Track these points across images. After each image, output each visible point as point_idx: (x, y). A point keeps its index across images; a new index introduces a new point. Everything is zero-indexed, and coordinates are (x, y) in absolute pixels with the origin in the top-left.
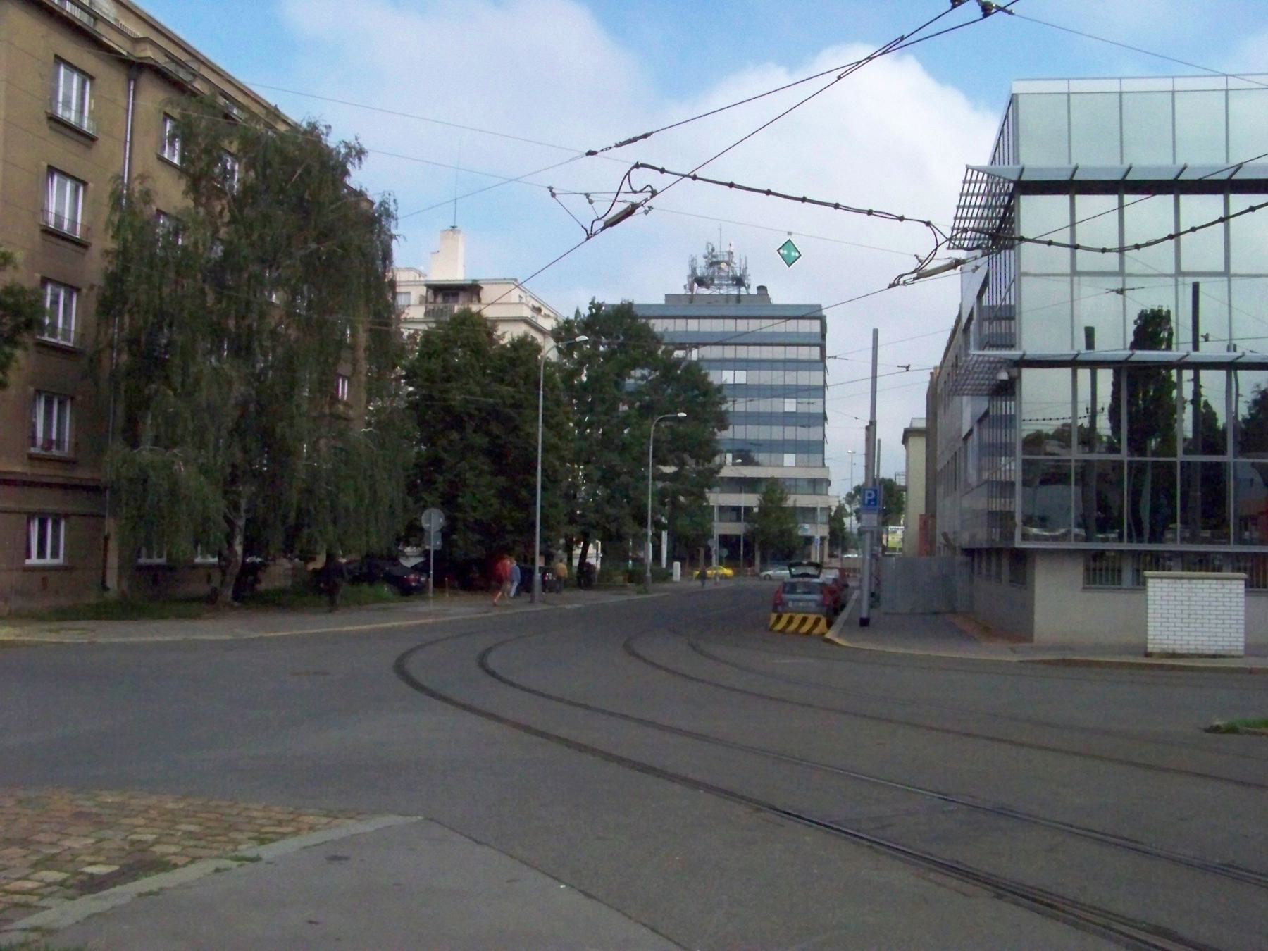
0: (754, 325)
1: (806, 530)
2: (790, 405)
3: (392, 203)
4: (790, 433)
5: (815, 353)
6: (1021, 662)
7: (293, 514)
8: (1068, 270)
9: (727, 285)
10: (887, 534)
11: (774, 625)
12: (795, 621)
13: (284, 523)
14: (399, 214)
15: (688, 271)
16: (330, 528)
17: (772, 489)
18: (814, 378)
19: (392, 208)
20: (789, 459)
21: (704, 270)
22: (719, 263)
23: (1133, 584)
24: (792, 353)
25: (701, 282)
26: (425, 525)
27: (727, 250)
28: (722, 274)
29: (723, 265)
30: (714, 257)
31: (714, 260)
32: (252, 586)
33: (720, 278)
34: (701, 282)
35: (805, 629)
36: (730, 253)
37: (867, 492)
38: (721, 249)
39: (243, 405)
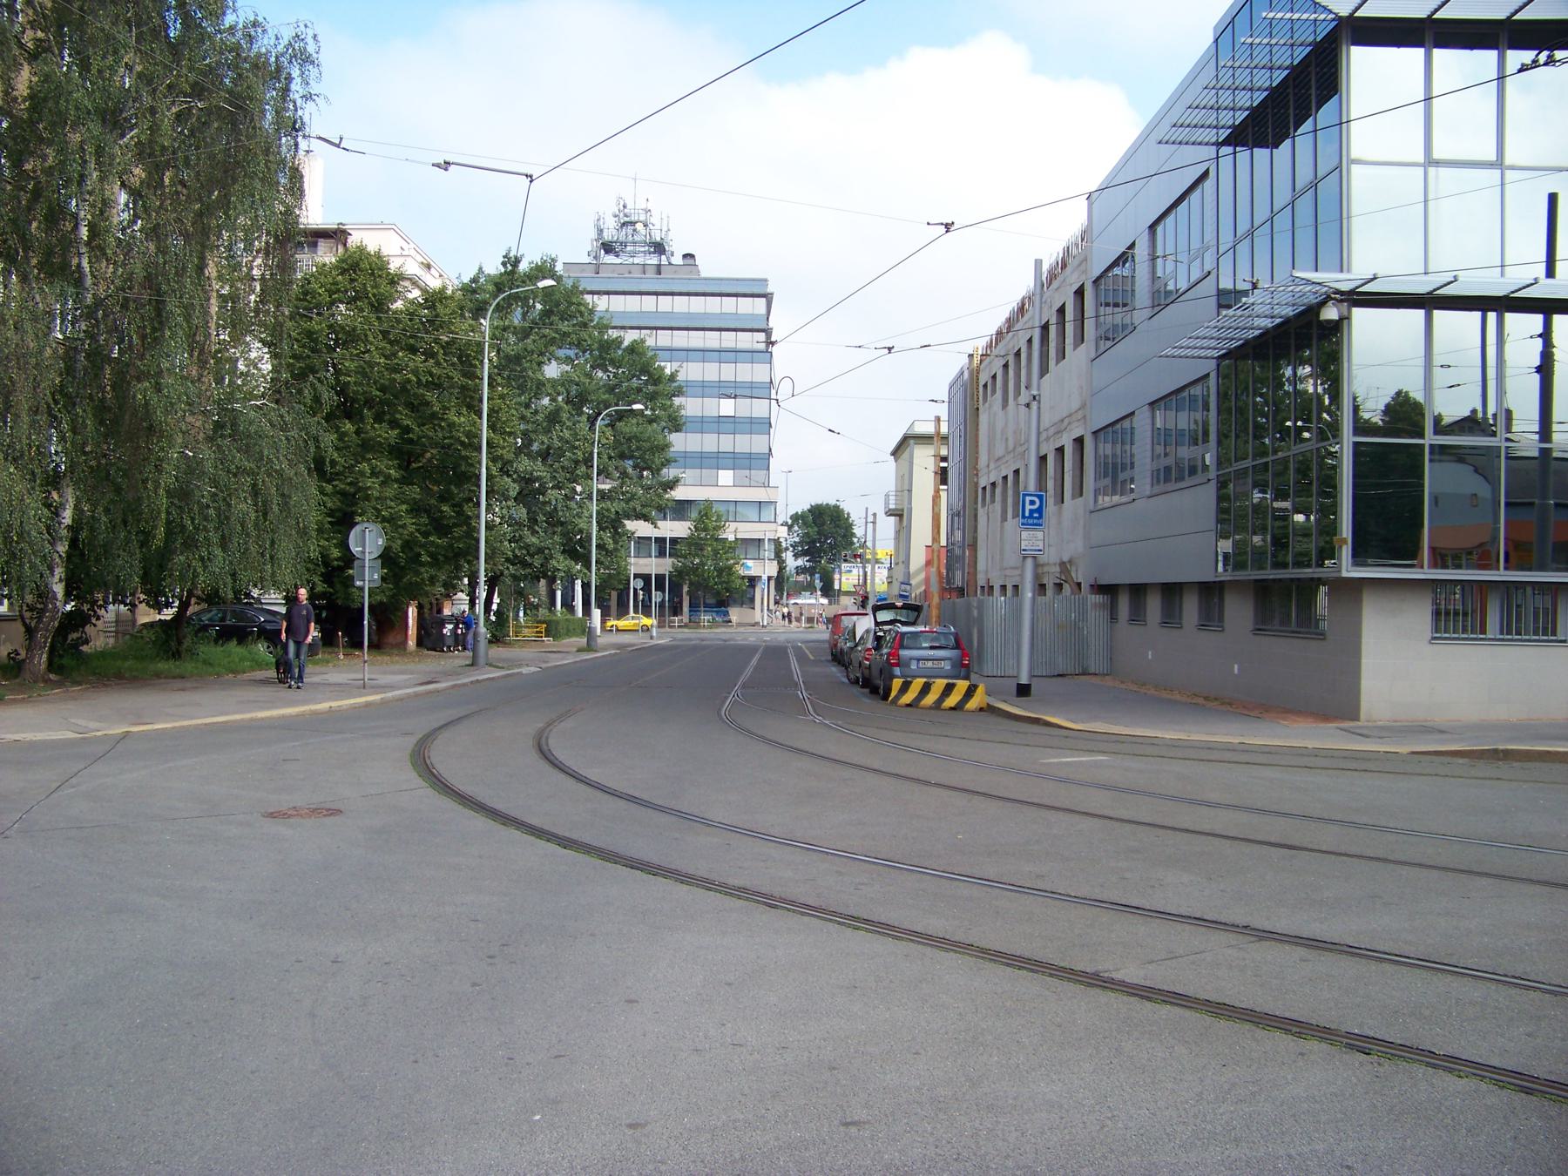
0: (681, 305)
1: (749, 568)
2: (727, 407)
3: (310, 40)
4: (726, 443)
5: (754, 341)
6: (1413, 753)
7: (160, 532)
8: (1421, 159)
9: (644, 252)
10: (840, 573)
11: (897, 697)
12: (934, 688)
13: (142, 545)
15: (593, 234)
16: (218, 551)
17: (706, 516)
18: (758, 373)
19: (311, 48)
20: (726, 477)
21: (615, 232)
22: (633, 223)
23: (1502, 633)
24: (729, 339)
25: (608, 248)
26: (356, 549)
27: (644, 206)
28: (637, 238)
29: (639, 226)
30: (626, 216)
31: (627, 219)
32: (76, 645)
33: (634, 243)
34: (608, 248)
35: (952, 701)
36: (647, 211)
37: (1028, 499)
38: (635, 209)
39: (70, 347)
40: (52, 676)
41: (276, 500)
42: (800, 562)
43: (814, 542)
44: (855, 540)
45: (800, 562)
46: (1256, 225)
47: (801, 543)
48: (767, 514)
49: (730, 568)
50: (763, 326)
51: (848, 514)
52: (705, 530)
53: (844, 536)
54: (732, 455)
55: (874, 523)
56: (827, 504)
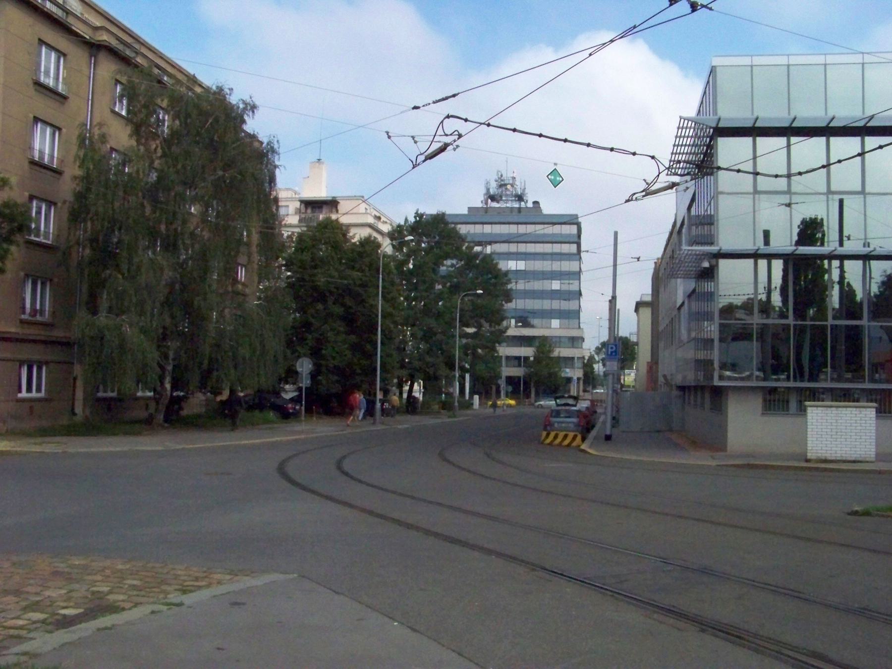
0: (530, 229)
1: (567, 373)
2: (556, 285)
3: (275, 143)
4: (556, 305)
5: (573, 248)
6: (718, 465)
7: (206, 362)
8: (751, 190)
9: (512, 201)
10: (624, 375)
11: (545, 440)
12: (559, 437)
13: (200, 368)
15: (484, 191)
16: (232, 371)
17: (543, 344)
18: (573, 266)
19: (276, 146)
20: (555, 323)
21: (495, 190)
22: (505, 185)
23: (797, 411)
24: (557, 248)
25: (493, 198)
26: (299, 369)
27: (512, 176)
29: (509, 187)
30: (502, 180)
31: (502, 183)
32: (177, 412)
33: (507, 195)
34: (493, 198)
35: (566, 442)
36: (514, 178)
37: (610, 346)
38: (507, 175)
40: (166, 425)
41: (259, 348)
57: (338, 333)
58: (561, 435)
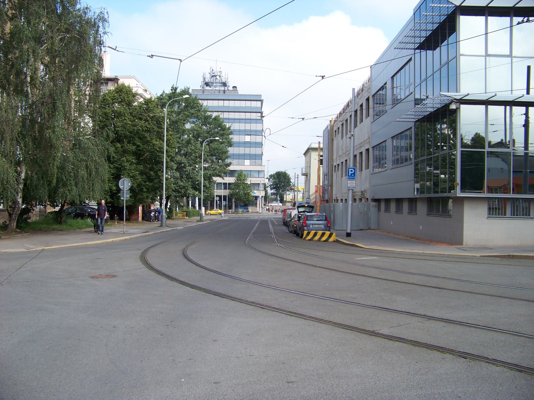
0: (232, 104)
1: (255, 193)
2: (248, 139)
3: (106, 14)
4: (247, 151)
5: (257, 116)
6: (481, 256)
8: (484, 54)
9: (219, 86)
10: (286, 195)
11: (306, 237)
12: (318, 234)
13: (49, 185)
14: (110, 20)
15: (202, 80)
16: (74, 188)
17: (240, 175)
18: (258, 127)
19: (106, 16)
20: (247, 162)
21: (209, 79)
22: (216, 76)
23: (511, 215)
24: (248, 115)
25: (207, 84)
26: (121, 187)
27: (219, 70)
29: (218, 77)
30: (213, 73)
31: (213, 75)
33: (216, 83)
34: (207, 84)
35: (324, 238)
36: (221, 72)
37: (350, 170)
38: (216, 71)
42: (272, 191)
43: (277, 184)
44: (291, 184)
45: (272, 191)
46: (428, 77)
47: (273, 185)
48: (261, 175)
49: (249, 193)
50: (260, 111)
51: (289, 175)
52: (240, 180)
53: (288, 182)
54: (249, 155)
55: (298, 178)
56: (282, 172)
57: (132, 163)
58: (320, 233)
